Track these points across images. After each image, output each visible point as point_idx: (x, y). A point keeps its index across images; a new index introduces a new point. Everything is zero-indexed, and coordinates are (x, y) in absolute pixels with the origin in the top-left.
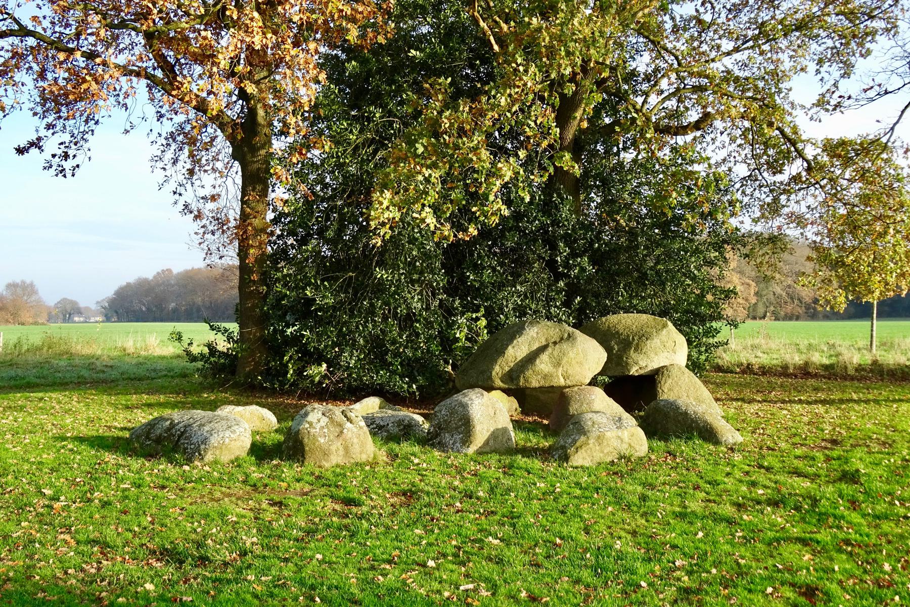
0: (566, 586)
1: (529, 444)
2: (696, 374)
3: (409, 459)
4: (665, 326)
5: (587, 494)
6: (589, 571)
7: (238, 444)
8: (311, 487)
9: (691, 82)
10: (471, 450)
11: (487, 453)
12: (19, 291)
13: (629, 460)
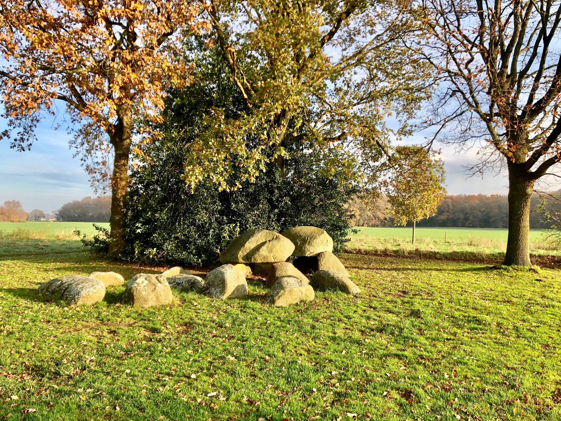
0: (270, 392)
1: (255, 293)
2: (336, 255)
3: (191, 303)
4: (323, 233)
5: (284, 324)
6: (284, 379)
7: (97, 295)
8: (134, 321)
9: (337, 118)
10: (225, 297)
11: (233, 298)
12: (11, 205)
13: (305, 303)
